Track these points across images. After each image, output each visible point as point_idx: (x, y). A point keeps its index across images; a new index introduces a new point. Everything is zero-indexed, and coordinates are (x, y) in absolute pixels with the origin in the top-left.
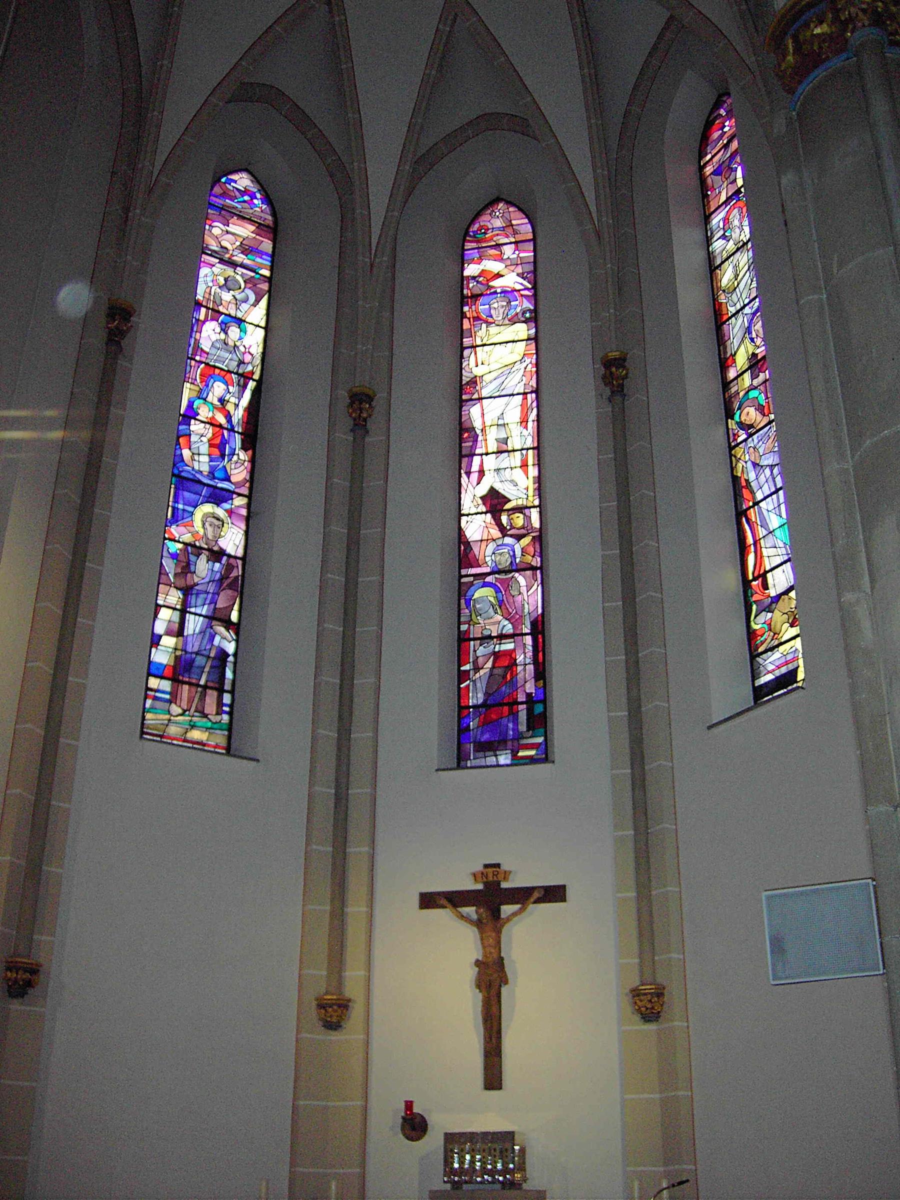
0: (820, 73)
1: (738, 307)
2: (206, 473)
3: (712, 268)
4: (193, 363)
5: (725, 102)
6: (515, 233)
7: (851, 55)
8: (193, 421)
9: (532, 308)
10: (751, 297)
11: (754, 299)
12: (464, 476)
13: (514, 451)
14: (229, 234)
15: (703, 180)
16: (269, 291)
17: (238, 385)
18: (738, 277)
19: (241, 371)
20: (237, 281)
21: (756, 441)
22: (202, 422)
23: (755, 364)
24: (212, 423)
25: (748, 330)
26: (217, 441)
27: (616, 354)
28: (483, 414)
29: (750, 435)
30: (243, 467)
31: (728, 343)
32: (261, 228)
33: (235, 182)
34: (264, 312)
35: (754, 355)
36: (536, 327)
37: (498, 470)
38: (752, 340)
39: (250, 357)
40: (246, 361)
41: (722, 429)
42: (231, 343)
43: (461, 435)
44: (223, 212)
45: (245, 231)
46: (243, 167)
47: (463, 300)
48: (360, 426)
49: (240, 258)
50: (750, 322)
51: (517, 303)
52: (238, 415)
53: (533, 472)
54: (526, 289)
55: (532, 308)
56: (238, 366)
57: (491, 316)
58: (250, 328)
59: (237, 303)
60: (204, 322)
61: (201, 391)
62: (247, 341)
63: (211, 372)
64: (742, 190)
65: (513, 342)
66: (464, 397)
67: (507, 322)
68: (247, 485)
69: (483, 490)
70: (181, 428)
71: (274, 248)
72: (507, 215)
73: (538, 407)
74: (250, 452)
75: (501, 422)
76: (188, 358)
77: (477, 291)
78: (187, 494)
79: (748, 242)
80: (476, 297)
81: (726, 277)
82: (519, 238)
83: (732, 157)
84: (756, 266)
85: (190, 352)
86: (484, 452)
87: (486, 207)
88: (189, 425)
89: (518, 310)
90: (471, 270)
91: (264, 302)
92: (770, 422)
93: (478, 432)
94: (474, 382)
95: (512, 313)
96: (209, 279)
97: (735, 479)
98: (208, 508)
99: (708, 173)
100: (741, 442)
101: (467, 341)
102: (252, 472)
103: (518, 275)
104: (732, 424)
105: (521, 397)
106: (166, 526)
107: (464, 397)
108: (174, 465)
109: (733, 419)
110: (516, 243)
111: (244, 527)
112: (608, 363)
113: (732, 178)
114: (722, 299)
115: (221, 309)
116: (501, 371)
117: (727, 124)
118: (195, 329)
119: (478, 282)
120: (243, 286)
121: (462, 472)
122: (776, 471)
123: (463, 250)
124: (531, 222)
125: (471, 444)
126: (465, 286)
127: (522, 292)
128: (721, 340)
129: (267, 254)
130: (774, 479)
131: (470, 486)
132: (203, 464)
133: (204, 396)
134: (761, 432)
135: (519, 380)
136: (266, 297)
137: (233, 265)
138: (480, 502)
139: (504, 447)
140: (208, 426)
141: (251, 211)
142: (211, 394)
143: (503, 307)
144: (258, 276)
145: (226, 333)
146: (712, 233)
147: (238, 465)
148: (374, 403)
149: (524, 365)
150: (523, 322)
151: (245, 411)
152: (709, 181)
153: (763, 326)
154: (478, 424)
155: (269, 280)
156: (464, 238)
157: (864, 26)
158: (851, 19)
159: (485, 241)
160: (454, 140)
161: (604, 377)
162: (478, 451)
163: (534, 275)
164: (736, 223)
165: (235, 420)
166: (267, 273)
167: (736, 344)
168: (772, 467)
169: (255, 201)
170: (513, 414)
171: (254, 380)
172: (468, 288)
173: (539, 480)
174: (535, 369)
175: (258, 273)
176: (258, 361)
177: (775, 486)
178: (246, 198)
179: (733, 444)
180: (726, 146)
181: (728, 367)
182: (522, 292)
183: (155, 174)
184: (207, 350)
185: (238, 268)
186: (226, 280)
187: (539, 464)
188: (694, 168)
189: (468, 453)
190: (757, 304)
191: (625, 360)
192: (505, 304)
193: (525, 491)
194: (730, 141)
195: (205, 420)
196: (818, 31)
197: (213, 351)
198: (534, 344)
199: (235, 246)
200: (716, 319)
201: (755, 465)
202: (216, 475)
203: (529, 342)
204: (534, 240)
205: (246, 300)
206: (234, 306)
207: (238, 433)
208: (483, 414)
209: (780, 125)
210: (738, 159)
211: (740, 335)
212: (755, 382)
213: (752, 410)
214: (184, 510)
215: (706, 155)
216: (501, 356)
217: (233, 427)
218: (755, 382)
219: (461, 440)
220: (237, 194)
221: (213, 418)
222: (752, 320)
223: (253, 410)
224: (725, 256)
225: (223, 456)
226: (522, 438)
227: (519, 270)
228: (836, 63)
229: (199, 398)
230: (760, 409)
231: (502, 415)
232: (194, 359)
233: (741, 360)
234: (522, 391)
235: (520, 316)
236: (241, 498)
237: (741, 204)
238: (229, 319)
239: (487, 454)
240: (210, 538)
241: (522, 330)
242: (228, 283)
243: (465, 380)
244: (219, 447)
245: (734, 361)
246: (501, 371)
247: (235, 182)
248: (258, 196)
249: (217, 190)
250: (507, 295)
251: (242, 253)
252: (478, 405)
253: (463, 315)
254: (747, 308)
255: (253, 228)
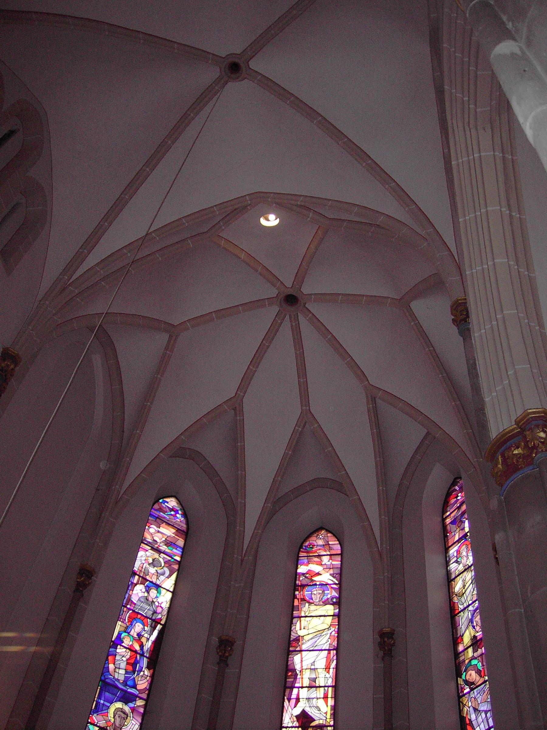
0: (518, 476)
1: (465, 605)
2: (122, 682)
3: (449, 580)
4: (125, 609)
5: (458, 482)
6: (330, 549)
7: (535, 467)
8: (119, 647)
9: (337, 596)
10: (473, 600)
11: (475, 601)
12: (286, 701)
13: (320, 687)
14: (159, 533)
15: (444, 526)
16: (178, 570)
17: (151, 626)
18: (465, 586)
19: (154, 618)
20: (160, 562)
21: (476, 693)
22: (125, 648)
23: (476, 643)
24: (130, 649)
25: (471, 621)
26: (132, 661)
27: (388, 630)
28: (302, 661)
29: (472, 689)
30: (146, 680)
31: (459, 628)
32: (179, 531)
33: (168, 502)
34: (174, 582)
35: (475, 637)
36: (339, 608)
37: (308, 699)
38: (474, 627)
39: (161, 609)
40: (158, 612)
41: (453, 685)
42: (150, 600)
43: (286, 673)
44: (158, 520)
45: (169, 532)
46: (174, 495)
47: (296, 587)
48: (223, 661)
49: (163, 548)
50: (473, 615)
51: (328, 592)
52: (148, 645)
53: (331, 702)
54: (336, 584)
55: (337, 596)
56: (153, 614)
57: (312, 599)
58: (163, 591)
59: (158, 575)
60: (136, 585)
61: (127, 628)
62: (160, 600)
63: (135, 616)
64: (468, 534)
65: (325, 616)
66: (291, 649)
67: (322, 604)
68: (147, 692)
69: (297, 711)
70: (111, 650)
71: (185, 544)
72: (326, 538)
73: (337, 659)
74: (152, 671)
75: (313, 667)
76: (123, 606)
77: (304, 583)
78: (107, 694)
79: (472, 565)
80: (303, 586)
81: (458, 587)
82: (333, 552)
83: (463, 513)
84: (477, 581)
85: (124, 602)
86: (300, 686)
87: (314, 532)
88: (116, 649)
89: (329, 596)
90: (302, 569)
91: (174, 576)
92: (485, 682)
93: (298, 672)
94: (298, 639)
95: (325, 598)
96: (143, 558)
97: (462, 719)
98: (119, 705)
99: (448, 523)
100: (466, 693)
101: (295, 613)
102: (151, 684)
103: (331, 575)
104: (460, 681)
105: (327, 652)
106: (91, 714)
107: (291, 649)
108: (102, 674)
109: (461, 678)
110: (330, 555)
111: (140, 720)
112: (382, 635)
113: (462, 527)
114: (455, 600)
115: (148, 577)
116: (315, 634)
117: (459, 495)
118: (130, 588)
119: (306, 577)
120: (163, 565)
121: (285, 698)
122: (489, 714)
123: (298, 557)
124: (340, 544)
125: (292, 680)
126: (298, 579)
127: (333, 586)
128: (454, 625)
129: (180, 547)
130: (487, 720)
131: (289, 708)
132: (120, 675)
133: (129, 631)
134: (479, 688)
135: (325, 641)
136: (176, 573)
137: (159, 551)
138: (295, 719)
139: (314, 684)
140: (128, 650)
141: (174, 521)
142: (133, 630)
143: (320, 593)
144: (173, 560)
145: (148, 593)
146: (449, 559)
147: (143, 678)
148: (234, 647)
149: (330, 631)
150: (331, 604)
151: (152, 643)
152: (448, 527)
153: (481, 619)
154: (298, 667)
155: (179, 563)
156: (299, 549)
157: (542, 451)
158: (534, 447)
159: (312, 552)
160: (299, 491)
161: (380, 644)
162: (297, 685)
163: (340, 575)
164: (464, 553)
165: (145, 648)
166: (178, 558)
167: (463, 629)
168: (486, 712)
169: (178, 515)
170: (321, 663)
171: (161, 624)
172: (299, 580)
173: (334, 708)
174: (336, 635)
175: (173, 558)
176: (165, 613)
177: (489, 725)
178: (173, 513)
179: (461, 694)
180: (459, 508)
181: (458, 643)
182: (333, 586)
183: (122, 493)
184: (135, 602)
185: (162, 554)
186: (153, 560)
187: (335, 697)
188: (440, 519)
189: (290, 685)
190: (477, 605)
191: (393, 634)
192: (321, 592)
193: (325, 715)
194: (462, 504)
195: (127, 646)
196: (516, 452)
197: (139, 603)
198: (337, 619)
199: (161, 541)
200: (451, 612)
201: (475, 710)
202: (128, 683)
203: (334, 617)
204: (341, 554)
205: (163, 574)
206: (155, 577)
207: (146, 657)
208: (302, 661)
209: (494, 504)
210: (466, 516)
211: (466, 623)
212: (476, 655)
213: (473, 673)
214: (103, 704)
215: (447, 512)
216: (316, 624)
217: (143, 653)
218: (476, 655)
219: (286, 677)
220: (167, 509)
221: (132, 645)
222: (474, 614)
223: (157, 643)
224: (457, 573)
225: (134, 671)
226: (326, 678)
227: (331, 571)
228: (527, 471)
229: (125, 632)
230: (479, 672)
231: (314, 663)
232: (126, 607)
233: (467, 639)
234: (327, 648)
235: (330, 600)
236: (141, 700)
237: (467, 542)
238: (151, 584)
239: (302, 687)
240: (117, 725)
241: (330, 609)
242: (155, 563)
243: (292, 637)
244: (133, 665)
245: (462, 640)
246: (315, 634)
247: (168, 502)
248: (180, 512)
249: (156, 506)
250: (322, 587)
251: (165, 545)
252: (299, 655)
253: (295, 597)
254: (471, 606)
255: (174, 531)
